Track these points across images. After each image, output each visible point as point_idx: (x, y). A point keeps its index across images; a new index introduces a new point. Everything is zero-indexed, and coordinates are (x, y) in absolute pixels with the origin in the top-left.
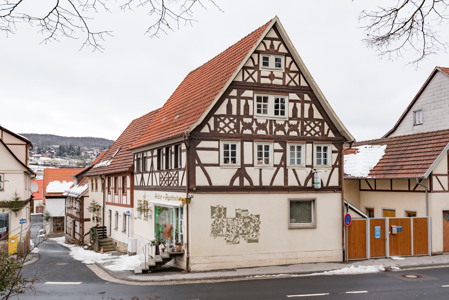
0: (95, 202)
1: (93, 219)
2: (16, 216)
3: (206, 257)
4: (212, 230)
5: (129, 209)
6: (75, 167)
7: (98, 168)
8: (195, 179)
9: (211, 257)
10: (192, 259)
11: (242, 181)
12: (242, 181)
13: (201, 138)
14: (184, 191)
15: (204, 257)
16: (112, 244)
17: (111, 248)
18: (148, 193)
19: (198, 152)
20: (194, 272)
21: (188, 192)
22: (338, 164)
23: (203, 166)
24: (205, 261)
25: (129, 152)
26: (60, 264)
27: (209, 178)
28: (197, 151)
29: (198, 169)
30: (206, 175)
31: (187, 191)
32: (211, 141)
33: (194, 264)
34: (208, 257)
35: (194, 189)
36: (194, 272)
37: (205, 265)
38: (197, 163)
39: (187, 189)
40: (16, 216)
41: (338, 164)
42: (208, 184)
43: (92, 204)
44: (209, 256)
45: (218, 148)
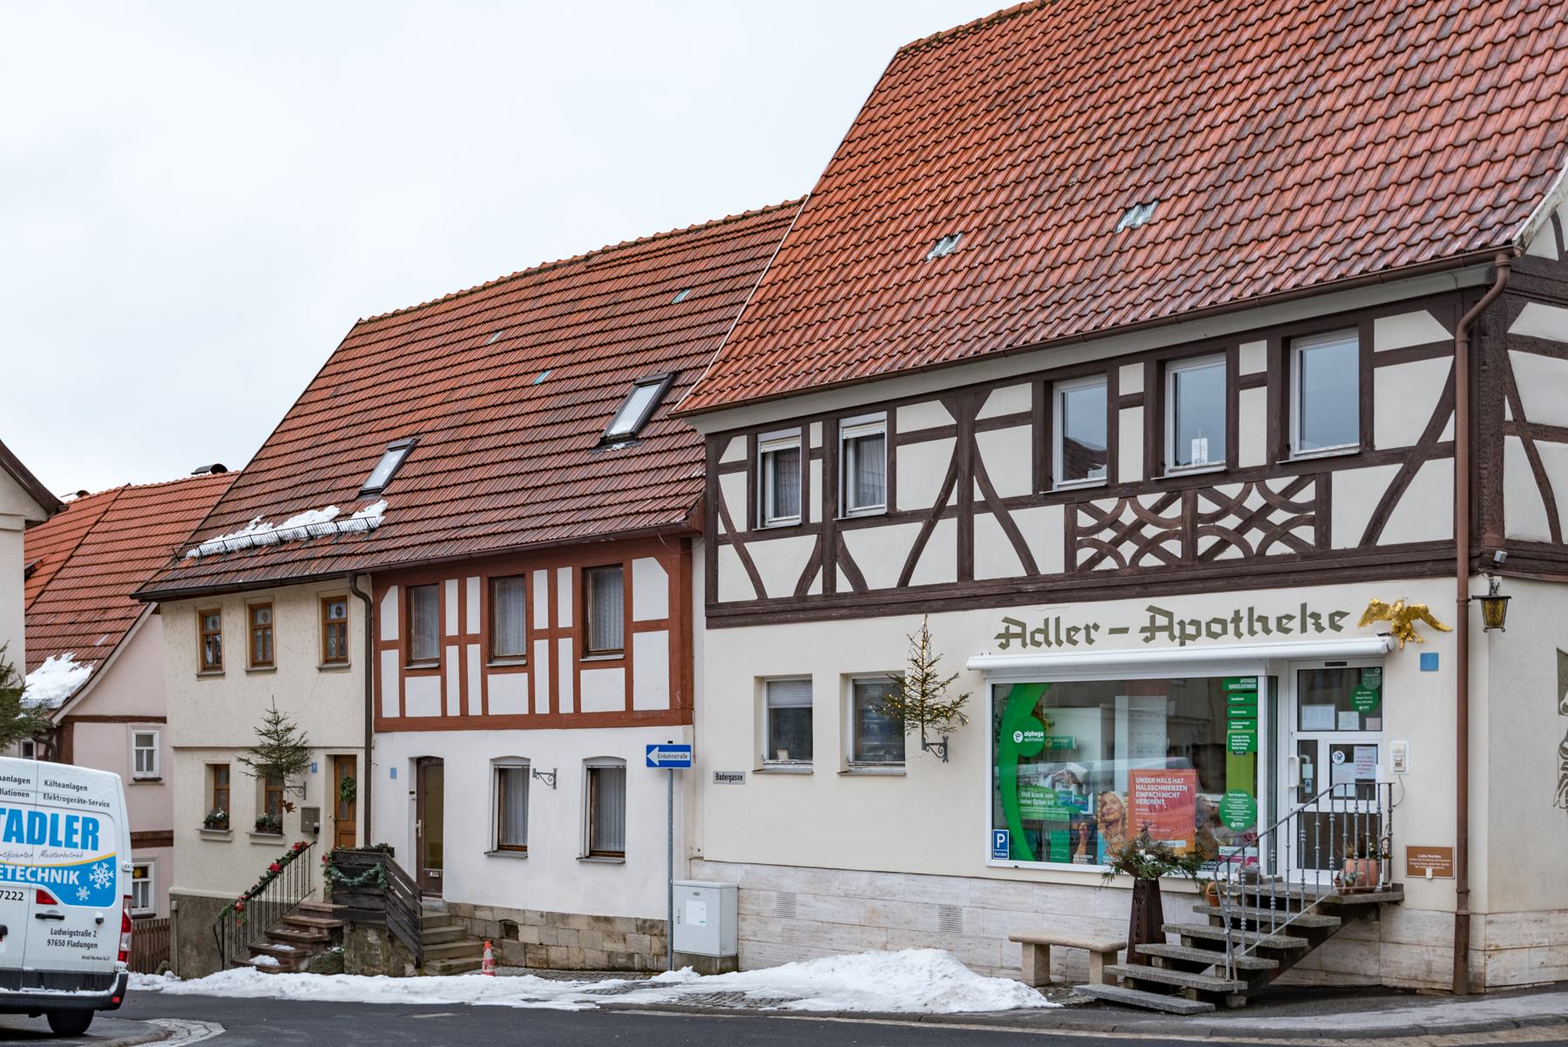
0: (289, 723)
1: (1188, 748)
2: (946, 759)
3: (1538, 916)
4: (1562, 773)
5: (676, 734)
6: (381, 526)
7: (297, 546)
8: (1502, 501)
9: (1556, 914)
10: (1490, 922)
11: (830, 581)
12: (830, 581)
13: (1528, 286)
14: (1441, 567)
15: (1532, 916)
16: (464, 935)
17: (471, 956)
18: (943, 624)
19: (1520, 360)
20: (1501, 992)
21: (1472, 572)
22: (953, 500)
23: (1532, 433)
24: (1535, 933)
25: (681, 425)
26: (913, 1024)
27: (1553, 499)
28: (1513, 354)
29: (1513, 446)
30: (1540, 484)
31: (1462, 565)
32: (1550, 303)
33: (1498, 950)
34: (1545, 916)
35: (1499, 555)
36: (1501, 992)
37: (1538, 957)
38: (1509, 416)
39: (1461, 553)
40: (946, 759)
41: (953, 500)
42: (1019, 571)
43: (267, 734)
44: (1549, 911)
45: (1029, 386)
